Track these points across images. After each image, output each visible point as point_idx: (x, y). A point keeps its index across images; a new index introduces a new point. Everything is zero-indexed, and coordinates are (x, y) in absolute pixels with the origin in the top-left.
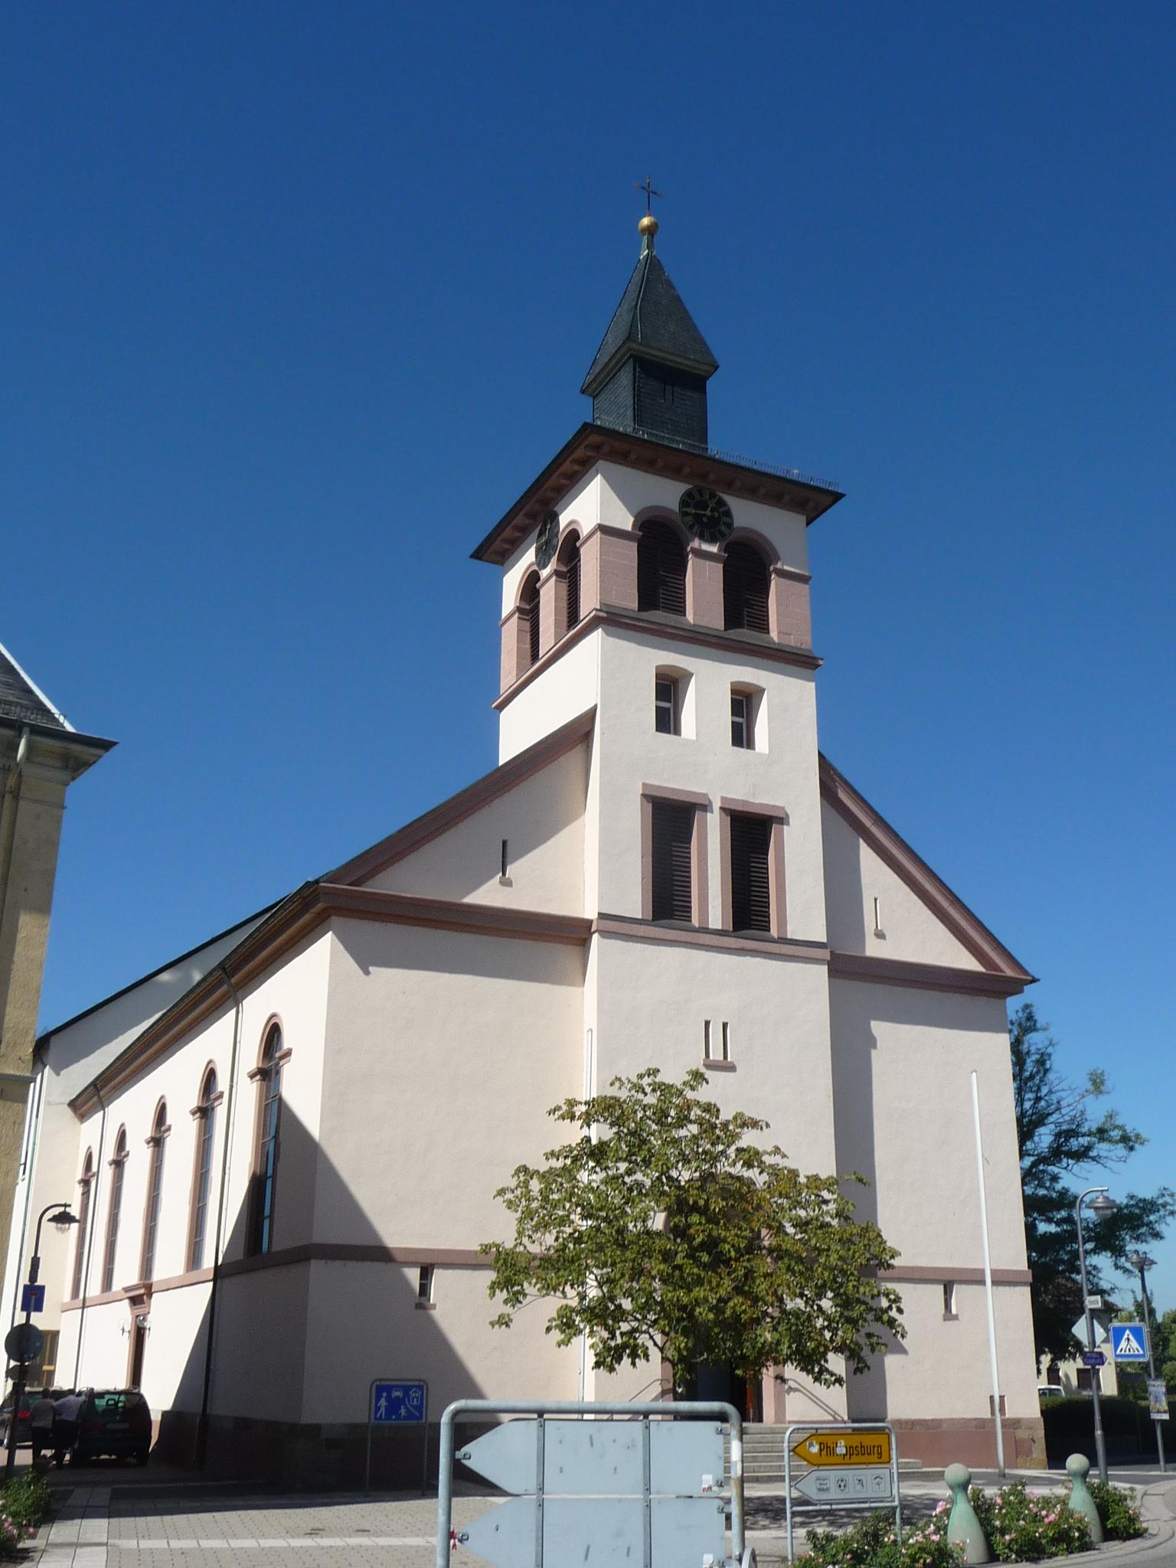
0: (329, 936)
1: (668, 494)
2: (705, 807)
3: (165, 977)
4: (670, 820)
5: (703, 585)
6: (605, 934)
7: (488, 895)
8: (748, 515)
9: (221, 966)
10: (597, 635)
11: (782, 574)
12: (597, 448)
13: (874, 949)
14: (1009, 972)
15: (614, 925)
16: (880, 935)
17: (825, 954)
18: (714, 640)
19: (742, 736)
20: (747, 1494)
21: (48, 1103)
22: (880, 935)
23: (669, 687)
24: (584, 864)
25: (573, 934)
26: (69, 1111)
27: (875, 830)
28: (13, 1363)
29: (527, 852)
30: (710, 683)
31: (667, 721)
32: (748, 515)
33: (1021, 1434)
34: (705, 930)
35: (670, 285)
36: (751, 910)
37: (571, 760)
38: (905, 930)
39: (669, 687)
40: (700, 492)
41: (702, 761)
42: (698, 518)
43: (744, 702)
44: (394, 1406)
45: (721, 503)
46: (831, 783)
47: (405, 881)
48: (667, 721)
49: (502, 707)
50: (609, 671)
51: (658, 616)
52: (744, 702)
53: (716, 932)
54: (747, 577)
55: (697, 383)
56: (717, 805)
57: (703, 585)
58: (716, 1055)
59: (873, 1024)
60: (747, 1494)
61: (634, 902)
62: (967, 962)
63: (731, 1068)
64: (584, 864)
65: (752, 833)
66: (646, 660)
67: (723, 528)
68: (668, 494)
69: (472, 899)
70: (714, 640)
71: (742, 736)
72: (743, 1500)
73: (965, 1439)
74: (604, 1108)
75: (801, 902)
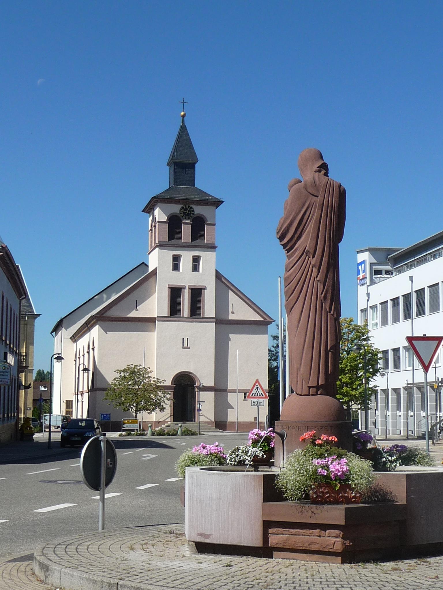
0: (98, 325)
1: (176, 209)
3: (96, 297)
4: (175, 293)
5: (186, 230)
6: (158, 321)
8: (198, 210)
9: (86, 323)
10: (157, 249)
12: (157, 201)
13: (231, 317)
14: (268, 320)
15: (161, 318)
16: (233, 313)
17: (215, 320)
19: (195, 268)
21: (64, 338)
22: (233, 313)
23: (176, 259)
24: (155, 304)
25: (152, 320)
26: (70, 340)
27: (232, 287)
28: (183, 384)
31: (176, 267)
33: (262, 425)
34: (183, 317)
36: (196, 311)
37: (152, 280)
38: (239, 311)
39: (176, 259)
40: (186, 206)
41: (185, 278)
43: (196, 260)
44: (104, 417)
45: (191, 208)
46: (219, 276)
47: (114, 313)
48: (176, 267)
49: (149, 254)
50: (160, 258)
51: (173, 242)
52: (196, 260)
53: (186, 318)
54: (199, 227)
55: (192, 166)
56: (187, 287)
57: (186, 230)
58: (185, 345)
59: (230, 335)
61: (165, 311)
62: (258, 318)
63: (189, 348)
64: (155, 304)
65: (197, 293)
66: (170, 254)
67: (192, 215)
68: (176, 209)
69: (128, 316)
71: (195, 268)
73: (247, 427)
74: (124, 371)
75: (209, 308)
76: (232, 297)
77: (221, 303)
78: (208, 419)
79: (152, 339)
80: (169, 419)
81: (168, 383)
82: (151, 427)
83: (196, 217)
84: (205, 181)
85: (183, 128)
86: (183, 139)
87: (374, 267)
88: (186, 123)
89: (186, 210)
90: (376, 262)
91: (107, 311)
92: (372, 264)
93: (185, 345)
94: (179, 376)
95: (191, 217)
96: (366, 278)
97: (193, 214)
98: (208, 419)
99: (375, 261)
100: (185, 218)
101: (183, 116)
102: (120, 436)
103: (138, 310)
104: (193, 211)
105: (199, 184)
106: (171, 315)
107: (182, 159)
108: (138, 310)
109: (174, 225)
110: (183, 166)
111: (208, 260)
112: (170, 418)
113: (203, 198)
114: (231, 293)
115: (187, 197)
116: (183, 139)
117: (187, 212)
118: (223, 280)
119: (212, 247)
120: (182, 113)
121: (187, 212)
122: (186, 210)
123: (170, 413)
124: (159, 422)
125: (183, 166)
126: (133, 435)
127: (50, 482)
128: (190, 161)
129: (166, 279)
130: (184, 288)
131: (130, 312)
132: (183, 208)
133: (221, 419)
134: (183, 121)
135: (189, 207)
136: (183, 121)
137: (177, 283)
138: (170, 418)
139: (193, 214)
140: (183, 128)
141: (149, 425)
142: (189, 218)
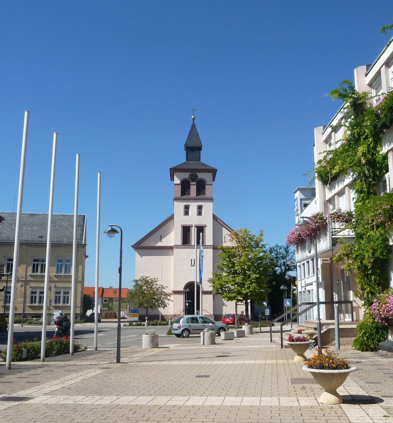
1: (186, 175)
2: (192, 226)
4: (186, 230)
5: (193, 189)
6: (175, 248)
7: (159, 244)
8: (201, 176)
11: (207, 185)
15: (177, 247)
16: (225, 242)
17: (212, 247)
18: (80, 274)
19: (200, 213)
20: (340, 327)
22: (225, 242)
23: (187, 208)
24: (173, 237)
25: (171, 248)
27: (224, 225)
29: (213, 210)
30: (193, 206)
31: (187, 213)
32: (201, 176)
34: (192, 246)
35: (196, 129)
37: (171, 222)
39: (187, 208)
40: (192, 174)
41: (193, 220)
42: (192, 178)
43: (200, 208)
45: (196, 175)
46: (215, 218)
47: (146, 244)
48: (187, 213)
51: (185, 197)
52: (200, 208)
53: (180, 245)
54: (201, 187)
55: (199, 149)
56: (194, 226)
57: (193, 189)
58: (193, 264)
60: (340, 327)
61: (179, 242)
65: (201, 229)
68: (186, 175)
69: (156, 245)
70: (80, 274)
71: (200, 213)
72: (339, 330)
75: (209, 239)
76: (225, 232)
77: (217, 236)
78: (209, 313)
79: (169, 261)
80: (182, 313)
81: (182, 289)
82: (171, 319)
83: (200, 180)
84: (207, 158)
85: (194, 126)
86: (193, 132)
87: (303, 202)
88: (195, 123)
89: (193, 176)
90: (304, 198)
91: (142, 242)
92: (301, 200)
93: (193, 264)
94: (188, 285)
95: (196, 180)
96: (298, 210)
97: (197, 178)
98: (209, 313)
99: (304, 197)
100: (192, 181)
101: (194, 119)
102: (124, 326)
103: (162, 242)
104: (197, 176)
105: (203, 160)
106: (183, 244)
107: (192, 144)
108: (162, 242)
109: (185, 187)
110: (193, 149)
111: (208, 208)
112: (183, 313)
113: (203, 167)
114: (224, 229)
115: (193, 167)
116: (193, 132)
117: (193, 178)
118: (218, 220)
119: (210, 199)
120: (193, 117)
121: (193, 178)
122: (193, 176)
123: (183, 309)
124: (175, 315)
125: (193, 149)
126: (134, 325)
127: (219, 344)
128: (197, 145)
129: (180, 220)
130: (192, 227)
131: (157, 242)
132: (190, 175)
133: (218, 313)
134: (193, 122)
135: (194, 174)
136: (193, 122)
137: (187, 223)
138: (183, 313)
139: (197, 178)
140: (194, 126)
141: (170, 318)
142: (194, 181)
